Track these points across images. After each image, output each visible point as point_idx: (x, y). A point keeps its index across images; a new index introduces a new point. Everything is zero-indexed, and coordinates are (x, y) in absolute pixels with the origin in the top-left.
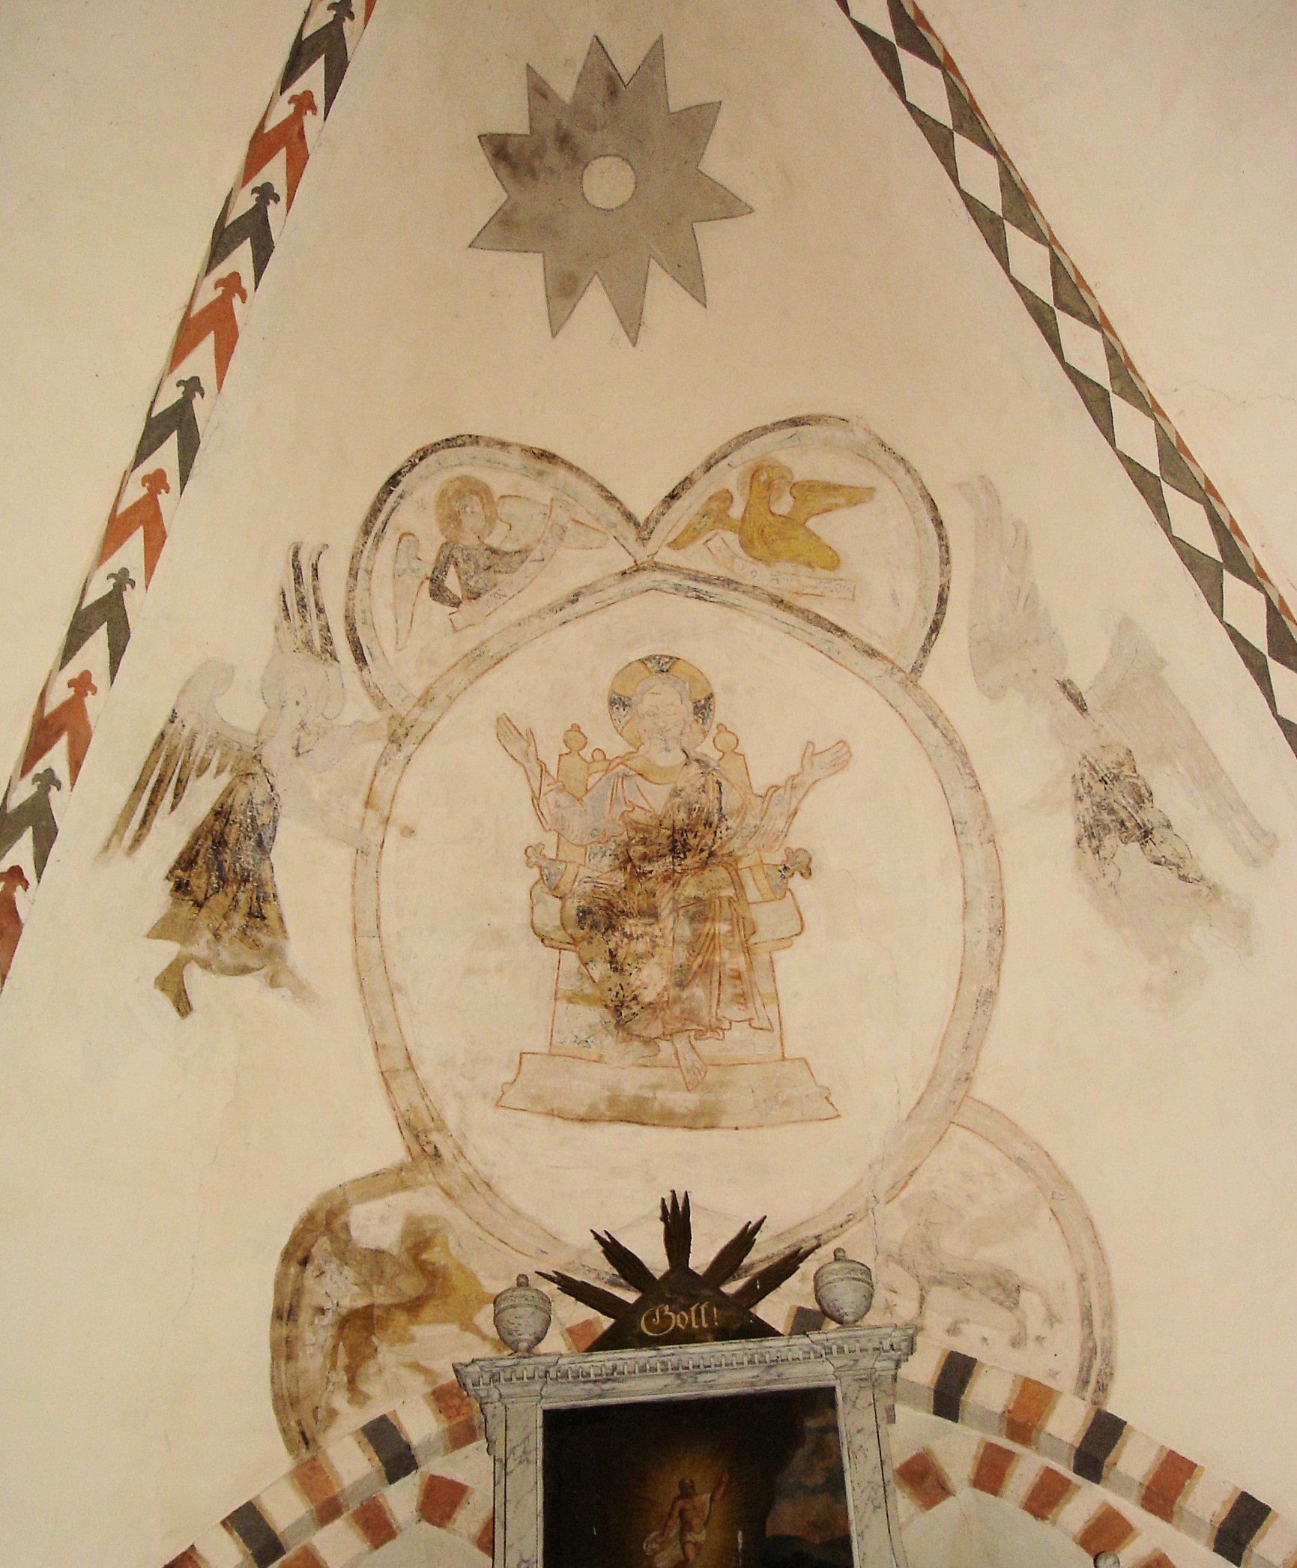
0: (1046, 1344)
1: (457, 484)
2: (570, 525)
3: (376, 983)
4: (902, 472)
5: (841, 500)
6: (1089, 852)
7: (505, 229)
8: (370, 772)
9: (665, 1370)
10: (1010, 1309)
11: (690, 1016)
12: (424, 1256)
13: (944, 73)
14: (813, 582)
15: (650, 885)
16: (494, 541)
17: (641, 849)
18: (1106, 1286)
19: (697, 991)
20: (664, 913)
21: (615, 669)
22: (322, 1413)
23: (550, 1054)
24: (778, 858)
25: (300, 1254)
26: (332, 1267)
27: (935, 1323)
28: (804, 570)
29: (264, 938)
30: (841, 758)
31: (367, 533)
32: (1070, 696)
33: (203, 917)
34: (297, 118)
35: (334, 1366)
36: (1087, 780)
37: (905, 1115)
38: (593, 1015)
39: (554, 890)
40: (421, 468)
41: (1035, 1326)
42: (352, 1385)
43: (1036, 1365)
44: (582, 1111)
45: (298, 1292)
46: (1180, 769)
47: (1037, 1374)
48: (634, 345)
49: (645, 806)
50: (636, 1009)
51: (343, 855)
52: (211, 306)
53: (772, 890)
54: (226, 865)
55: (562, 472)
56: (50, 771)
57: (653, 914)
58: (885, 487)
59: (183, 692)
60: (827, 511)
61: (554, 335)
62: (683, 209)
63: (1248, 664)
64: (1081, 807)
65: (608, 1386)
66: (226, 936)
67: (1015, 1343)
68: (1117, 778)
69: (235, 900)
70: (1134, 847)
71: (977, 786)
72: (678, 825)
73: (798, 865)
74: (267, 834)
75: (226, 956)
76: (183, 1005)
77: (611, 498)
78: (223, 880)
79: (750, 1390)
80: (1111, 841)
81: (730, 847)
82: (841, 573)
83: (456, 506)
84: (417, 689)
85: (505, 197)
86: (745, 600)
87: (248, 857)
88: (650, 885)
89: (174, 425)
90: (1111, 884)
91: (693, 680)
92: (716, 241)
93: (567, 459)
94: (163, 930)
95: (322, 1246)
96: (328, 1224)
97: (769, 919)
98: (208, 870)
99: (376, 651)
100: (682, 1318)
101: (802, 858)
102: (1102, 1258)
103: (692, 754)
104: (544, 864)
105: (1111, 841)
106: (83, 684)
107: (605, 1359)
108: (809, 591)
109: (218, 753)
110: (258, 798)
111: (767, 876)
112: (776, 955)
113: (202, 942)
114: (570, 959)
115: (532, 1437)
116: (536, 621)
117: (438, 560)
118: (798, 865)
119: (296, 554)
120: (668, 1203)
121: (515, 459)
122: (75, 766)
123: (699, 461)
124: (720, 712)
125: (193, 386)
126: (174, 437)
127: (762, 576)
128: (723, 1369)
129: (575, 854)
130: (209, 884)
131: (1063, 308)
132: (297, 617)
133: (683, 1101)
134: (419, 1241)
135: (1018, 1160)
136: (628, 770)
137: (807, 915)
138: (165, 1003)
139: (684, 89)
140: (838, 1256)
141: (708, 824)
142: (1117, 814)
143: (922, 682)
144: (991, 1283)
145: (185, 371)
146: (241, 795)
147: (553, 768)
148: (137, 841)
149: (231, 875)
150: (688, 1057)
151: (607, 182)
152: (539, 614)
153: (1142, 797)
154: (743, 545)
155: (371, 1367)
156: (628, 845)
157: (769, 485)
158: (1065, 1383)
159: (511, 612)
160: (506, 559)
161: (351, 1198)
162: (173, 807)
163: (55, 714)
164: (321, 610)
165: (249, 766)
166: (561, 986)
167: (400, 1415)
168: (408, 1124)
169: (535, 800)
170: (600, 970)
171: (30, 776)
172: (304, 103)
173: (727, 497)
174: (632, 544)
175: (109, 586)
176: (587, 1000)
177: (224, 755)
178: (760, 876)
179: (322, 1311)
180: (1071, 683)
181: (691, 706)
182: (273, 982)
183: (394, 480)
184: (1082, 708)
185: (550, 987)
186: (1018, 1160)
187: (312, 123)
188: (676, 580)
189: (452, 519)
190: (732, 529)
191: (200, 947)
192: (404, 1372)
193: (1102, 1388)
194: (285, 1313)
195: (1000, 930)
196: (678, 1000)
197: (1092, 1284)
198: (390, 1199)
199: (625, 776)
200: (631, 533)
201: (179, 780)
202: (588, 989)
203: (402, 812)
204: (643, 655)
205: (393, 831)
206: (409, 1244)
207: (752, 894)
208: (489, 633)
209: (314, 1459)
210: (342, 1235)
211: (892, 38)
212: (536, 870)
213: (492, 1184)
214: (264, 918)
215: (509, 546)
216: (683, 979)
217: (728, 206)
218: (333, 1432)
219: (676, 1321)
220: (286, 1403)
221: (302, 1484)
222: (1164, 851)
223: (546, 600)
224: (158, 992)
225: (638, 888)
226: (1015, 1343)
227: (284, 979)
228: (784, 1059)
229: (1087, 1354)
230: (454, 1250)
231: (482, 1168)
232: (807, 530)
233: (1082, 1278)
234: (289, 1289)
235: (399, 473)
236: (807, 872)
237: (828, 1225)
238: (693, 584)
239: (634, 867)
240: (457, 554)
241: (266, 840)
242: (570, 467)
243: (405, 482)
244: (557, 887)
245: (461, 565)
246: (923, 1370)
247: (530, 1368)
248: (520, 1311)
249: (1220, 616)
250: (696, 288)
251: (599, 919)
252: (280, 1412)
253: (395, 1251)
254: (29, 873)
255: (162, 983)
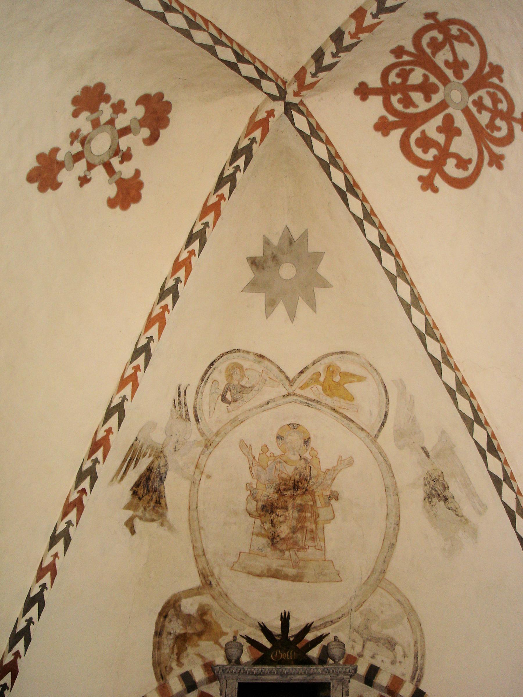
0: (402, 664)
1: (232, 365)
2: (268, 379)
3: (195, 526)
4: (375, 373)
5: (356, 380)
6: (428, 503)
7: (253, 286)
8: (198, 457)
9: (277, 673)
10: (392, 651)
11: (296, 543)
12: (205, 618)
13: (395, 258)
14: (345, 405)
15: (286, 499)
16: (243, 383)
17: (284, 487)
18: (423, 646)
19: (299, 535)
20: (290, 508)
21: (279, 427)
22: (168, 669)
23: (250, 553)
24: (328, 493)
25: (164, 614)
26: (174, 619)
27: (367, 654)
28: (342, 400)
29: (160, 510)
30: (350, 462)
31: (202, 380)
32: (425, 452)
33: (141, 503)
34: (189, 257)
35: (173, 653)
36: (428, 479)
37: (363, 583)
38: (263, 541)
39: (255, 498)
40: (221, 360)
41: (399, 658)
42: (178, 660)
43: (398, 671)
44: (258, 573)
45: (163, 626)
46: (458, 480)
47: (398, 674)
48: (292, 323)
49: (286, 472)
50: (278, 539)
51: (187, 484)
52: (159, 314)
53: (325, 503)
54: (150, 486)
55: (266, 362)
56: (96, 459)
57: (286, 508)
58: (370, 377)
59: (140, 431)
60: (351, 382)
61: (267, 318)
62: (310, 284)
63: (480, 453)
64: (426, 488)
65: (259, 677)
66: (148, 509)
67: (393, 663)
68: (438, 480)
69: (152, 497)
70: (442, 503)
71: (393, 476)
72: (296, 479)
73: (335, 496)
74: (164, 476)
75: (147, 516)
76: (133, 531)
77: (282, 371)
78: (148, 491)
79: (303, 681)
80: (435, 500)
81: (312, 488)
82: (354, 403)
83: (232, 372)
84: (215, 431)
85: (254, 276)
86: (323, 408)
87: (156, 484)
88: (286, 499)
89: (143, 351)
90: (434, 514)
91: (304, 432)
92: (320, 294)
93: (268, 357)
94: (128, 507)
95: (172, 612)
96: (174, 604)
97: (323, 512)
98: (144, 488)
99: (203, 418)
100: (284, 655)
101: (335, 494)
102: (423, 636)
103: (302, 457)
104: (252, 490)
105: (435, 500)
106: (109, 431)
107: (258, 668)
108: (343, 407)
109: (150, 450)
110: (161, 465)
111: (324, 499)
112: (326, 525)
113: (140, 511)
114: (258, 522)
115: (234, 692)
116: (254, 410)
117: (224, 389)
118: (335, 496)
119: (179, 388)
120: (283, 614)
121: (252, 357)
122: (105, 457)
123: (310, 361)
124: (312, 444)
125: (151, 339)
126: (144, 354)
127: (329, 401)
128: (297, 674)
129: (261, 487)
130: (144, 492)
131: (428, 335)
132: (178, 407)
133: (291, 571)
134: (203, 612)
135: (399, 601)
136: (281, 460)
137: (336, 513)
138: (127, 531)
139: (313, 246)
140: (336, 639)
141: (306, 480)
142: (437, 492)
143: (378, 441)
144: (386, 642)
145: (148, 334)
146: (156, 463)
147: (257, 458)
148: (122, 478)
149: (151, 490)
150: (294, 557)
151: (287, 271)
152: (256, 408)
153: (445, 487)
154: (323, 390)
155: (185, 654)
156: (279, 485)
157: (333, 372)
158: (407, 678)
159: (247, 406)
160: (246, 389)
161: (182, 596)
162: (134, 467)
163: (100, 440)
164: (186, 405)
165: (159, 454)
166: (255, 530)
167: (193, 671)
168: (202, 573)
169: (250, 468)
170: (267, 526)
171: (90, 460)
172: (192, 253)
173: (319, 374)
174: (288, 387)
175: (120, 401)
176: (262, 535)
177: (151, 451)
178: (321, 498)
179: (170, 634)
180: (425, 448)
181: (303, 441)
182: (162, 524)
183: (212, 364)
184: (428, 456)
185: (251, 531)
186: (399, 601)
187: (194, 259)
188: (300, 399)
189: (230, 376)
190: (320, 384)
191: (140, 513)
192: (195, 657)
193: (419, 681)
194: (158, 634)
195: (398, 524)
196: (292, 538)
197: (419, 645)
198: (195, 598)
199: (280, 462)
200: (287, 383)
201: (137, 459)
202: (263, 532)
203: (207, 470)
204: (288, 423)
205: (204, 476)
206: (200, 613)
207: (319, 504)
208: (239, 413)
209: (164, 684)
210: (178, 609)
211: (379, 246)
212: (249, 492)
213: (228, 595)
214: (160, 504)
215: (247, 385)
216: (294, 530)
217: (325, 284)
218: (171, 676)
219: (282, 656)
220: (157, 664)
221: (160, 692)
222: (451, 505)
223: (259, 403)
224: (125, 527)
225: (282, 500)
226: (393, 663)
227: (165, 523)
228: (325, 560)
229: (415, 669)
230: (214, 616)
231: (225, 590)
232: (344, 387)
233: (416, 642)
234: (160, 625)
235: (214, 361)
236: (337, 499)
237: (335, 617)
238: (306, 401)
239: (281, 492)
240: (231, 387)
241: (163, 478)
242: (269, 360)
243: (216, 364)
244: (256, 498)
245: (232, 391)
246: (362, 670)
247: (235, 669)
248: (233, 650)
249: (472, 436)
250: (313, 306)
251: (268, 509)
252: (154, 667)
253: (195, 615)
254: (88, 490)
255: (126, 524)
